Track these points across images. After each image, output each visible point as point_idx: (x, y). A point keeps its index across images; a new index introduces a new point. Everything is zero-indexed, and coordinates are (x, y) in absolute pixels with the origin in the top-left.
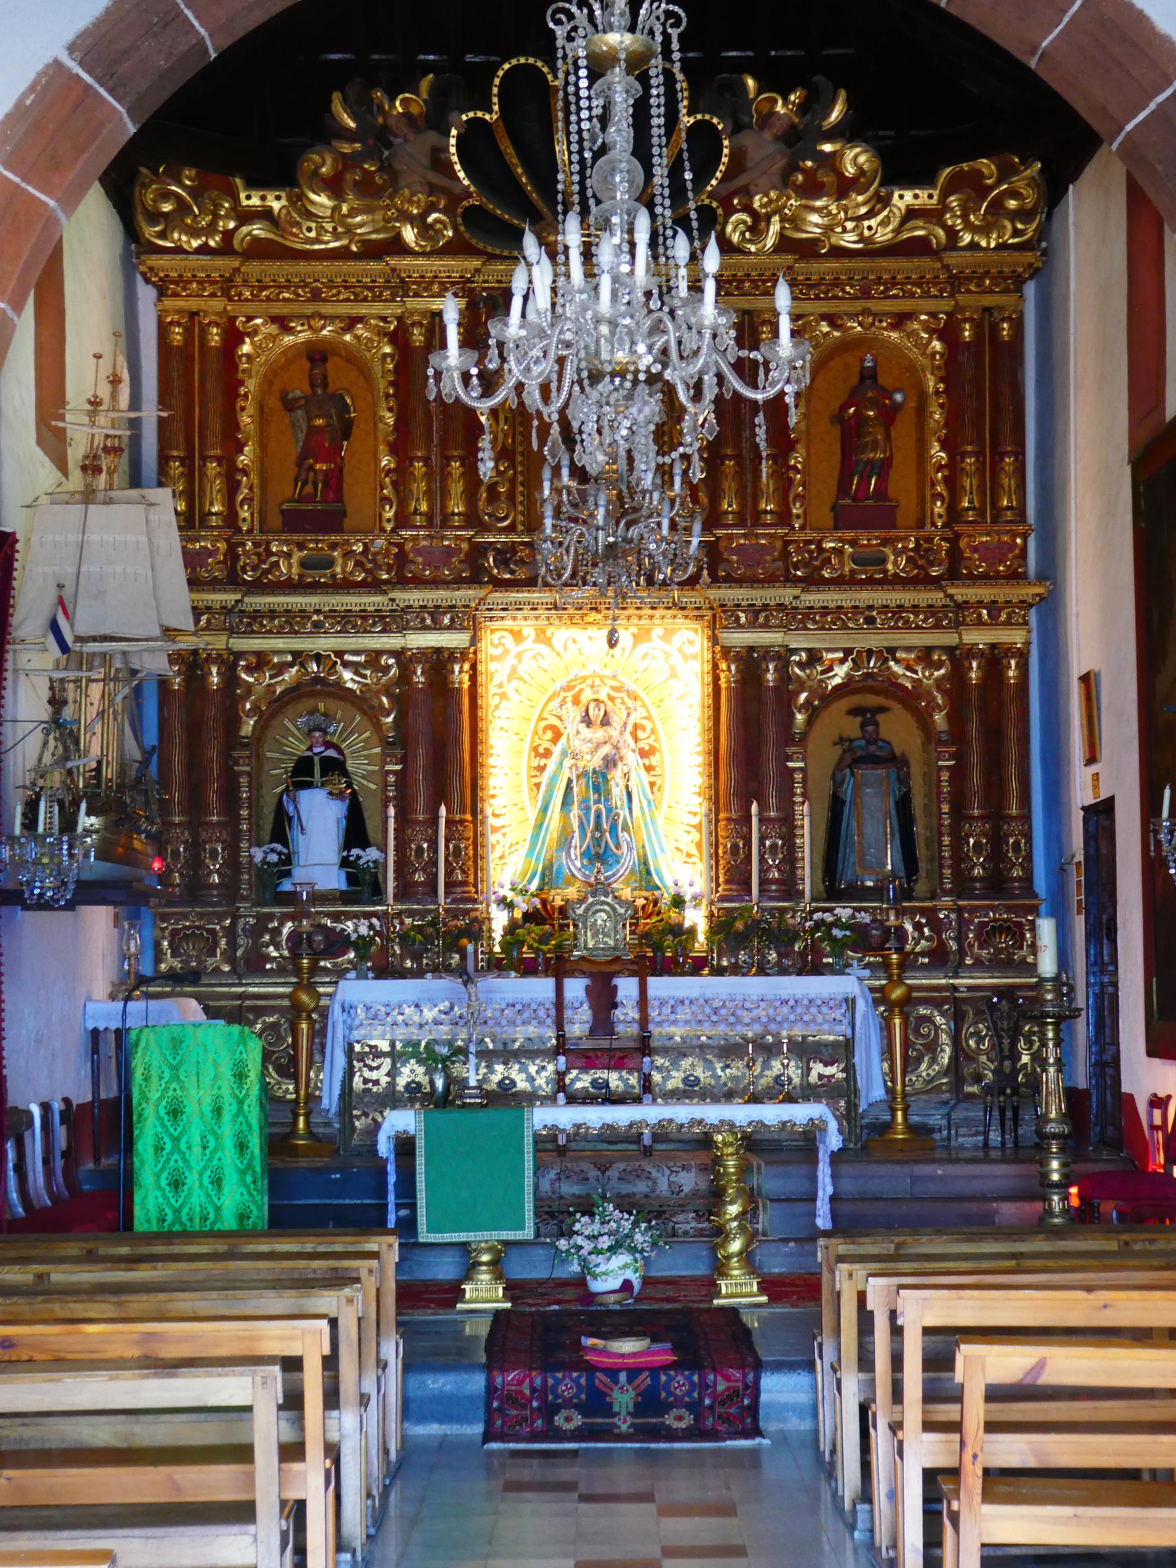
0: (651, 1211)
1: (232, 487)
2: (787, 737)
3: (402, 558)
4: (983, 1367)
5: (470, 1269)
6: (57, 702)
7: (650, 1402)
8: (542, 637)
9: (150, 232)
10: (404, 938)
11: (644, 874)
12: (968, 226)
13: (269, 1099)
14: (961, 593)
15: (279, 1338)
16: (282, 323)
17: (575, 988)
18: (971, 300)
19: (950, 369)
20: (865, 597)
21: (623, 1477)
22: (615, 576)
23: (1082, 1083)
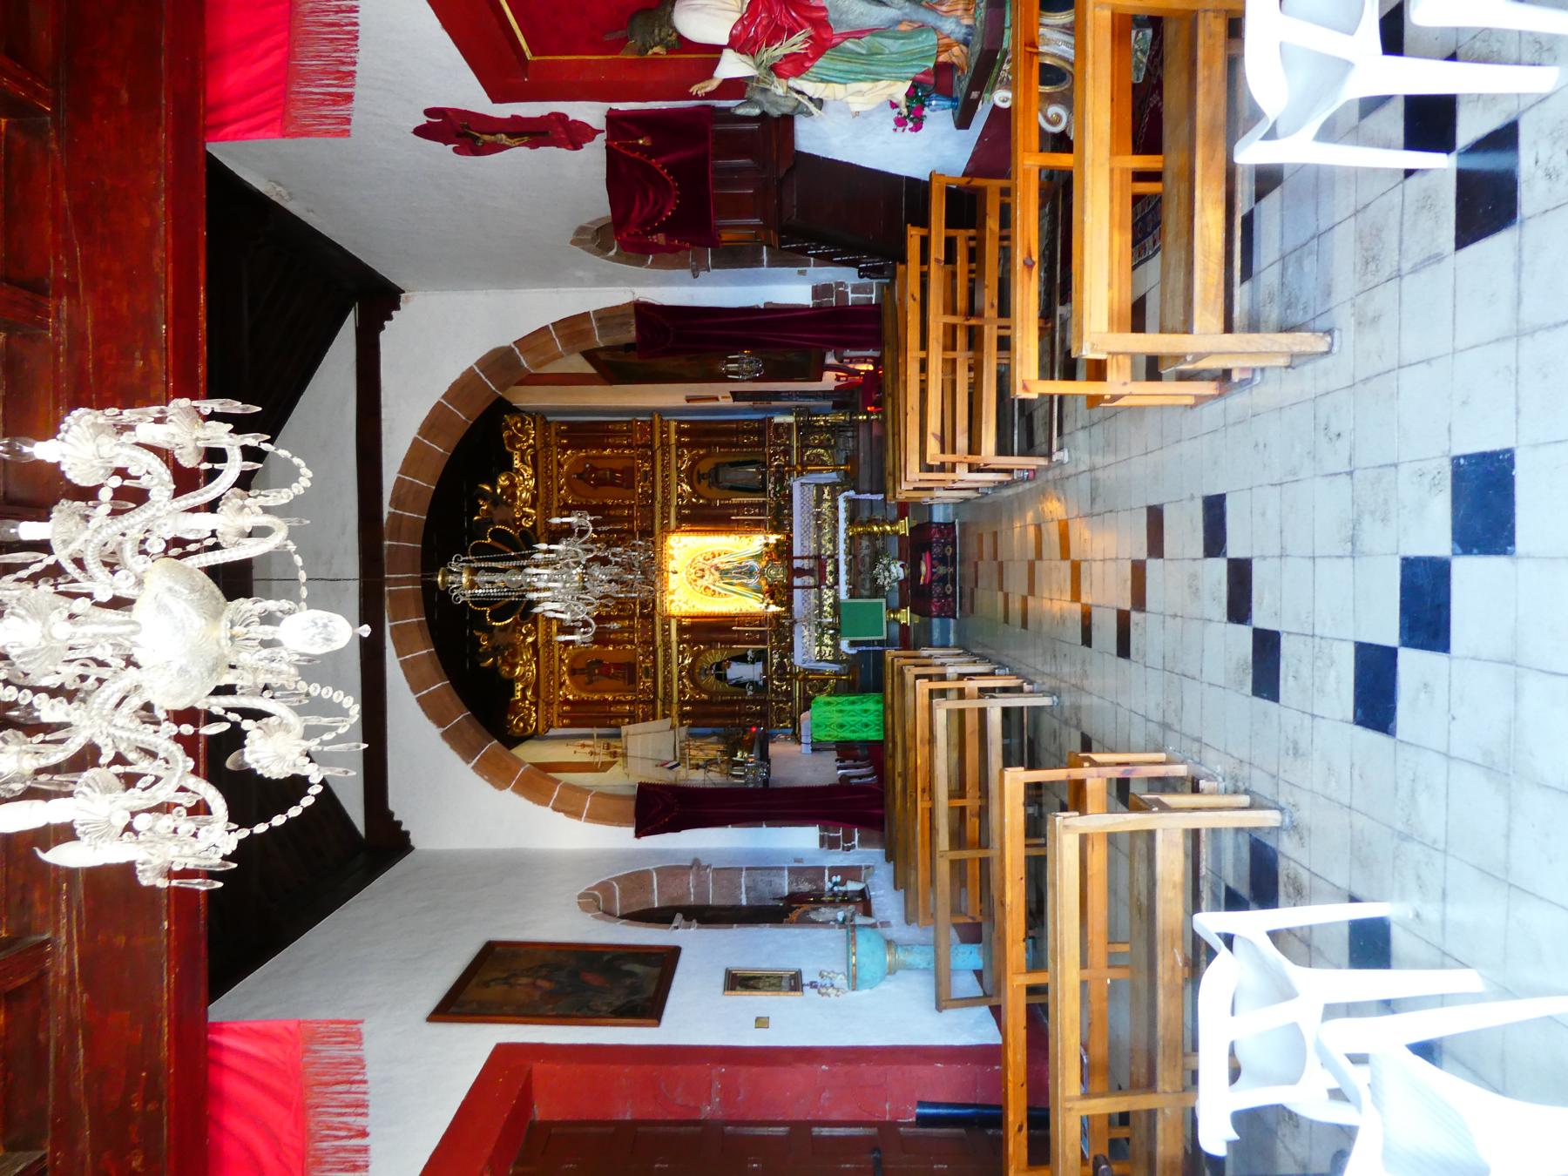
1: (620, 702)
2: (708, 506)
3: (645, 642)
4: (934, 452)
6: (698, 767)
7: (943, 560)
8: (672, 593)
9: (530, 731)
11: (757, 557)
13: (836, 692)
16: (562, 684)
17: (797, 582)
18: (553, 440)
19: (577, 447)
20: (658, 477)
22: (652, 571)
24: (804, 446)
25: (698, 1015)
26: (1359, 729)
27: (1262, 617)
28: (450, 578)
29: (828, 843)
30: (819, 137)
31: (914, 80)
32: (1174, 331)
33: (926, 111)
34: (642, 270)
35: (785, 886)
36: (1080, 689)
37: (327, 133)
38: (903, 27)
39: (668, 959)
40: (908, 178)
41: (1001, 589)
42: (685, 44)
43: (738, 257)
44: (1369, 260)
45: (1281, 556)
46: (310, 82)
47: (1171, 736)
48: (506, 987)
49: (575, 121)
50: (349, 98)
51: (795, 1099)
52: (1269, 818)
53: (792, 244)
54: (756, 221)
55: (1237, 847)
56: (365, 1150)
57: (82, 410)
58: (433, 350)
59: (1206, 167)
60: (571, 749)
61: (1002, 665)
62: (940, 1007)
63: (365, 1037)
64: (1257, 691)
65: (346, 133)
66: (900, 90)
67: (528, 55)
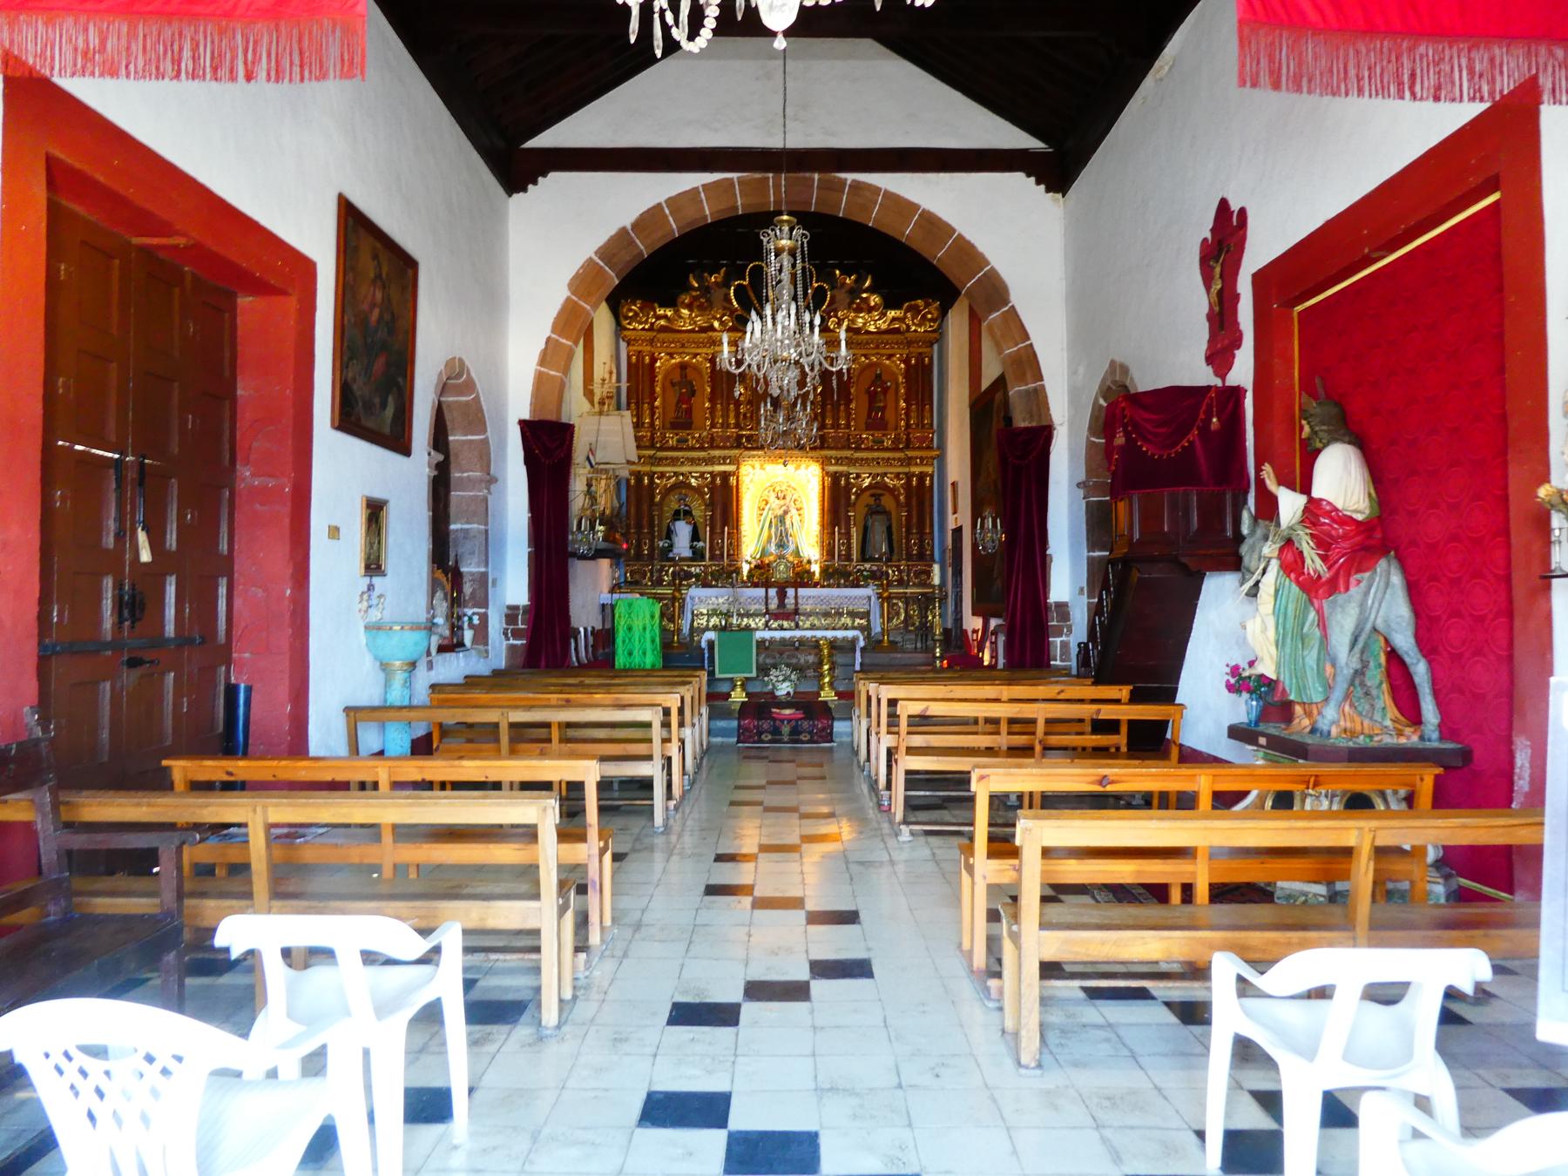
0: (799, 669)
1: (653, 414)
2: (848, 504)
3: (712, 439)
4: (906, 710)
5: (734, 688)
6: (589, 485)
7: (795, 732)
8: (762, 468)
9: (625, 323)
10: (712, 573)
11: (797, 553)
13: (664, 630)
14: (910, 454)
15: (659, 698)
16: (671, 355)
17: (773, 592)
18: (915, 350)
19: (907, 374)
20: (876, 455)
21: (786, 755)
22: (787, 446)
23: (949, 626)
24: (907, 600)
25: (343, 469)
26: (644, 1096)
27: (750, 1010)
28: (786, 228)
29: (512, 614)
30: (1219, 596)
31: (1276, 682)
32: (1041, 915)
33: (1245, 695)
34: (1085, 433)
35: (469, 568)
36: (670, 853)
37: (1242, 66)
38: (1329, 669)
39: (399, 442)
40: (1176, 690)
41: (771, 783)
42: (1310, 457)
43: (1099, 524)
44: (1112, 1100)
45: (814, 1028)
46: (1291, 49)
47: (628, 933)
48: (372, 275)
49: (1233, 356)
50: (1276, 86)
51: (256, 557)
52: (550, 1015)
53: (1111, 577)
54: (1137, 536)
55: (518, 990)
56: (233, 77)
58: (1005, 224)
59: (1202, 941)
60: (607, 360)
61: (692, 783)
62: (348, 710)
63: (347, 83)
64: (676, 1006)
65: (1242, 83)
66: (1267, 668)
67: (1299, 308)
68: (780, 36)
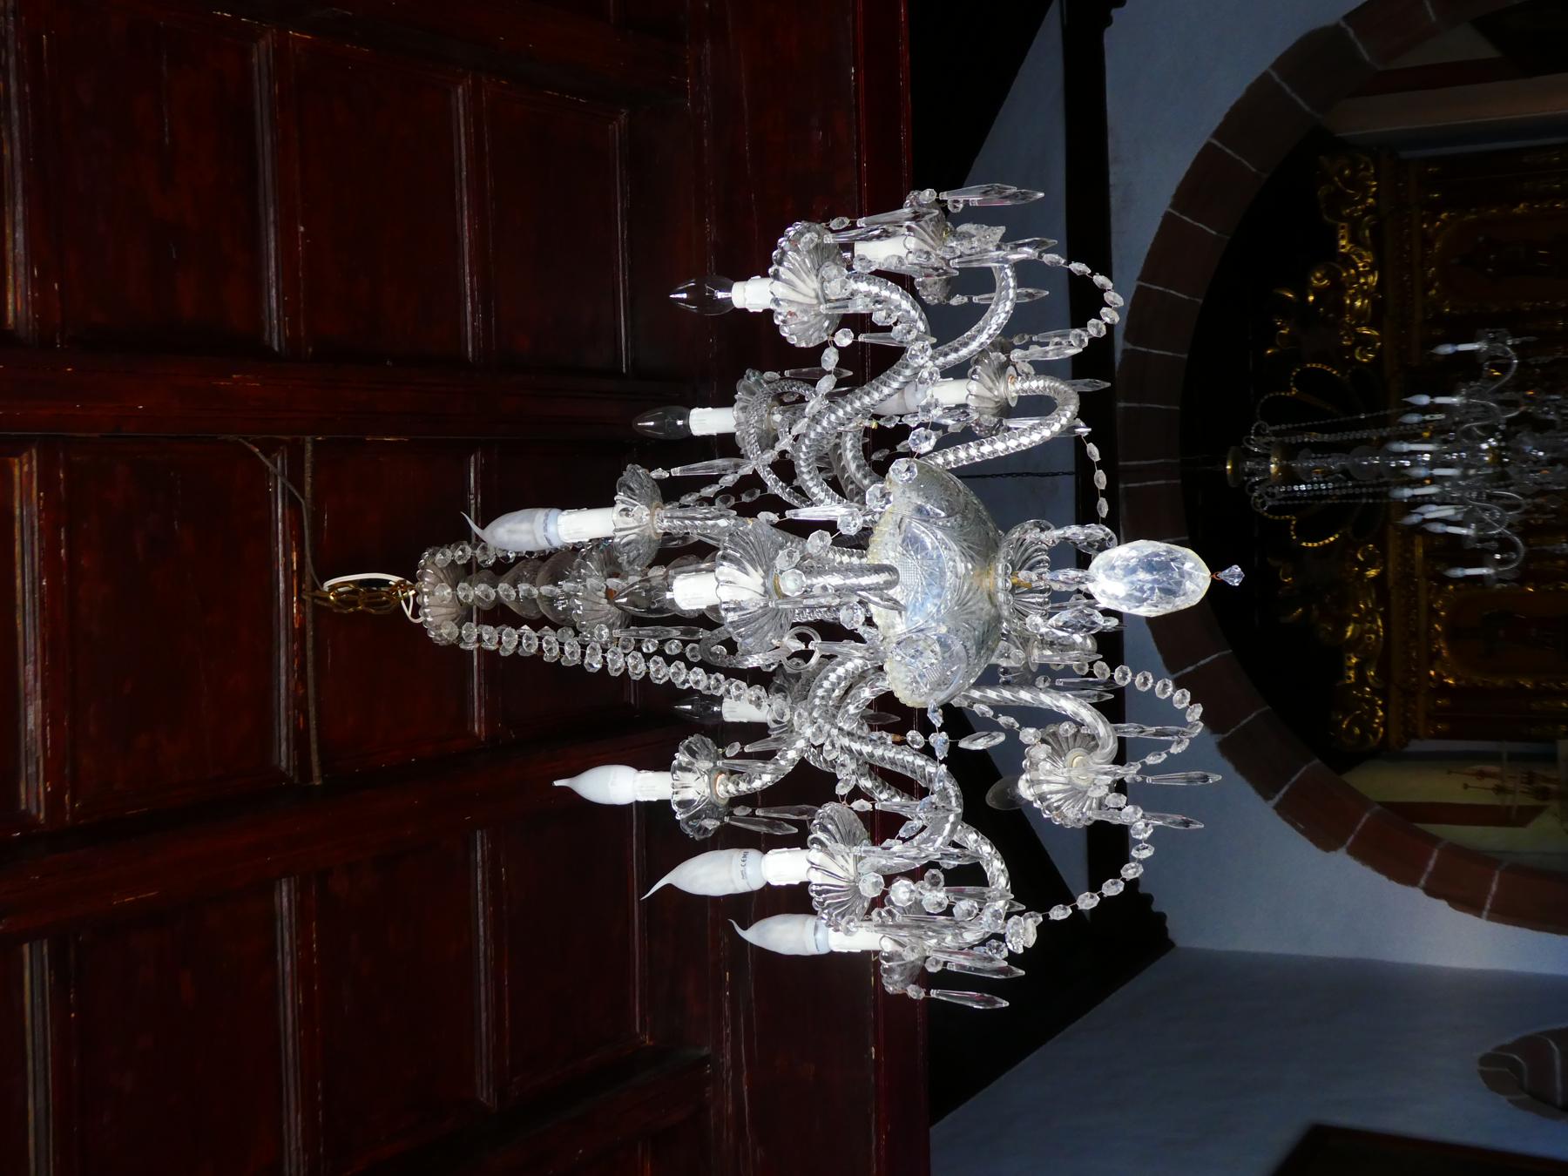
12: (1363, 201)
16: (1433, 658)
57: (799, 226)
68: (1222, 575)
